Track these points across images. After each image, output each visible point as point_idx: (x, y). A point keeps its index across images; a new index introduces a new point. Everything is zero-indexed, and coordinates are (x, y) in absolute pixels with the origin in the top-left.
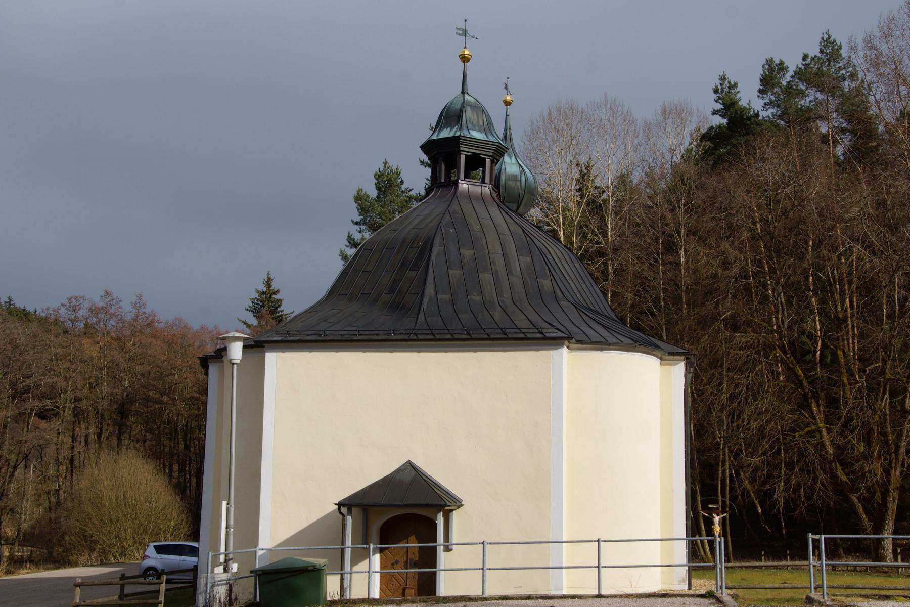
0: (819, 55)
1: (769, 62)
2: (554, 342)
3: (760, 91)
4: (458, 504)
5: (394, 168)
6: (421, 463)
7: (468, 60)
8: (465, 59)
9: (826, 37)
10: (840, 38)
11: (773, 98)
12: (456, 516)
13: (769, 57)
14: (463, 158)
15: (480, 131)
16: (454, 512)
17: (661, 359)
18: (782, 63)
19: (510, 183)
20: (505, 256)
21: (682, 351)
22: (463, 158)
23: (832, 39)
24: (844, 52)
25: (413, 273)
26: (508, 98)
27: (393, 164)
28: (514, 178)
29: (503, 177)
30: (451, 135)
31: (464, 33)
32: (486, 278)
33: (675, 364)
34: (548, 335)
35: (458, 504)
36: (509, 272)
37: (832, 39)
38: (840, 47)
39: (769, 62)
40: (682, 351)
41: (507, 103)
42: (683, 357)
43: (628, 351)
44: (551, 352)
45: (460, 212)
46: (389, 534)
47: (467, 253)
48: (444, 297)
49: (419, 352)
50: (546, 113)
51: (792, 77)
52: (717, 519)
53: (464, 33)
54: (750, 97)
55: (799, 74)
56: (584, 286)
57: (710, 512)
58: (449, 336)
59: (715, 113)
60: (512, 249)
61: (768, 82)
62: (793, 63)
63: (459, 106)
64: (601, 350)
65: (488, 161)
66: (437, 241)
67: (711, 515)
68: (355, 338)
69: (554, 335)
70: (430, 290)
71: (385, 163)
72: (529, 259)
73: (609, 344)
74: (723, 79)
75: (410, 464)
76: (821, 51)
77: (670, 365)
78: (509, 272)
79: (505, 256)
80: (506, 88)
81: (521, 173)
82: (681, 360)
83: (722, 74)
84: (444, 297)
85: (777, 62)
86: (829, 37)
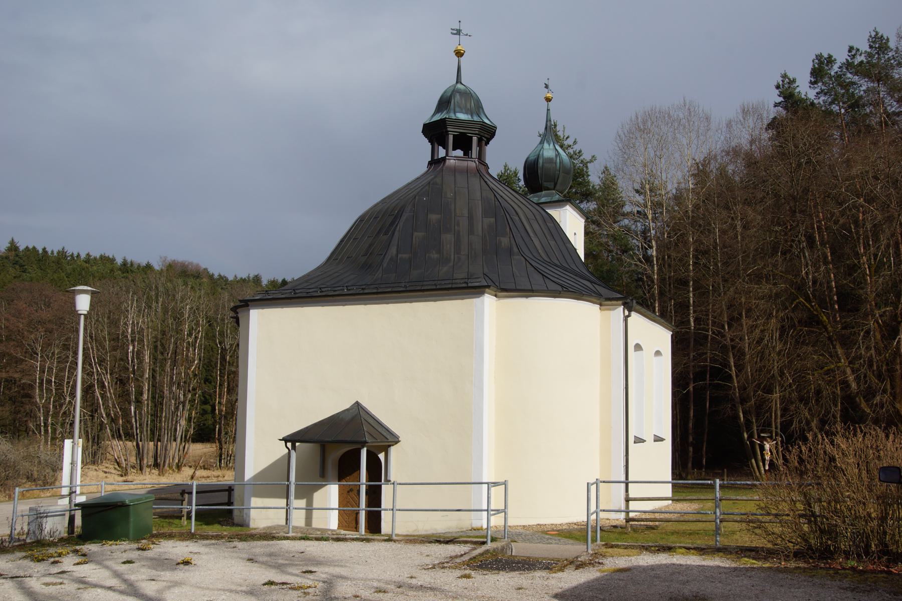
0: (869, 50)
1: (819, 57)
2: (476, 290)
3: (811, 82)
4: (396, 440)
5: (513, 169)
6: (365, 403)
7: (462, 55)
8: (459, 54)
9: (873, 34)
10: (884, 32)
11: (823, 88)
12: (393, 450)
13: (818, 53)
14: (451, 138)
15: (466, 113)
16: (392, 448)
17: (601, 305)
18: (830, 57)
19: (547, 166)
20: (471, 218)
21: (620, 296)
22: (451, 138)
23: (880, 35)
24: (892, 44)
26: (549, 95)
28: (550, 160)
29: (541, 161)
31: (458, 32)
32: (448, 238)
33: (614, 309)
35: (396, 440)
36: (471, 231)
37: (880, 35)
38: (888, 40)
39: (819, 57)
40: (620, 296)
41: (548, 100)
42: (620, 302)
43: (555, 297)
44: (474, 300)
46: (346, 469)
49: (365, 304)
50: (634, 118)
51: (840, 67)
52: (767, 446)
53: (458, 32)
54: (806, 90)
55: (848, 65)
56: (552, 243)
57: (762, 439)
59: (776, 105)
60: (479, 212)
61: (819, 72)
62: (841, 57)
64: (527, 297)
65: (475, 139)
67: (762, 442)
68: (316, 294)
70: (393, 250)
71: (505, 167)
72: (493, 220)
73: (537, 291)
74: (784, 76)
75: (357, 403)
76: (871, 47)
77: (610, 310)
78: (471, 231)
79: (471, 218)
80: (547, 86)
81: (556, 156)
82: (620, 305)
83: (783, 73)
85: (826, 56)
86: (877, 33)
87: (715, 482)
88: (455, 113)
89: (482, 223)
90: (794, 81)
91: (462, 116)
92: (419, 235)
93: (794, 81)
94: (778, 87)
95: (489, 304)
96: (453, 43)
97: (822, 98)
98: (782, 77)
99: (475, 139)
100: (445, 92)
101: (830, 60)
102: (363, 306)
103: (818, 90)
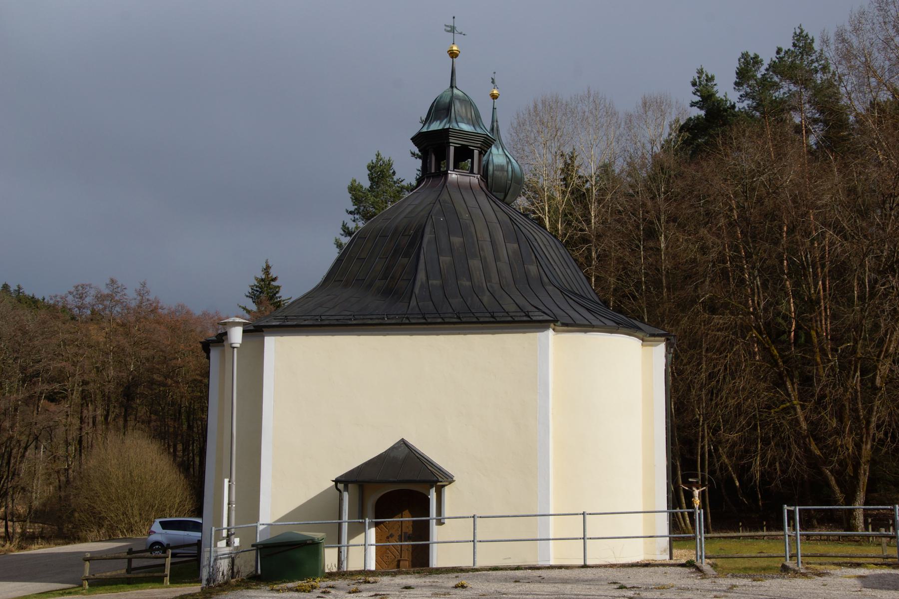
1: (745, 56)
3: (736, 84)
4: (450, 479)
5: (386, 159)
6: (412, 441)
7: (457, 55)
8: (453, 55)
9: (798, 31)
10: (813, 32)
11: (748, 90)
12: (447, 491)
13: (744, 51)
14: (452, 149)
15: (468, 123)
16: (446, 488)
17: (643, 340)
18: (756, 57)
20: (493, 243)
21: (663, 332)
22: (452, 149)
25: (405, 260)
26: (495, 92)
27: (385, 156)
28: (501, 168)
29: (491, 168)
30: (440, 127)
31: (453, 30)
33: (656, 346)
34: (534, 318)
35: (450, 479)
36: (497, 259)
38: (813, 40)
39: (745, 56)
40: (663, 332)
43: (611, 333)
45: (450, 201)
47: (456, 240)
48: (435, 282)
51: (767, 70)
52: (696, 492)
54: (727, 90)
55: (773, 67)
56: (569, 271)
58: (440, 320)
59: (693, 104)
60: (499, 236)
62: (768, 57)
63: (448, 100)
64: (586, 332)
65: (476, 152)
66: (428, 229)
69: (541, 318)
70: (421, 276)
71: (378, 155)
72: (516, 246)
74: (700, 72)
75: (403, 442)
76: (794, 45)
77: (652, 346)
78: (497, 259)
79: (493, 243)
80: (493, 82)
81: (508, 163)
83: (699, 68)
84: (435, 282)
86: (802, 32)
87: (895, 508)
88: (457, 123)
89: (508, 249)
90: (712, 79)
91: (465, 127)
92: (445, 259)
93: (712, 79)
94: (694, 84)
95: (552, 341)
96: (447, 42)
97: (746, 102)
98: (698, 73)
99: (476, 152)
100: (441, 97)
101: (756, 61)
102: (408, 337)
103: (742, 93)
